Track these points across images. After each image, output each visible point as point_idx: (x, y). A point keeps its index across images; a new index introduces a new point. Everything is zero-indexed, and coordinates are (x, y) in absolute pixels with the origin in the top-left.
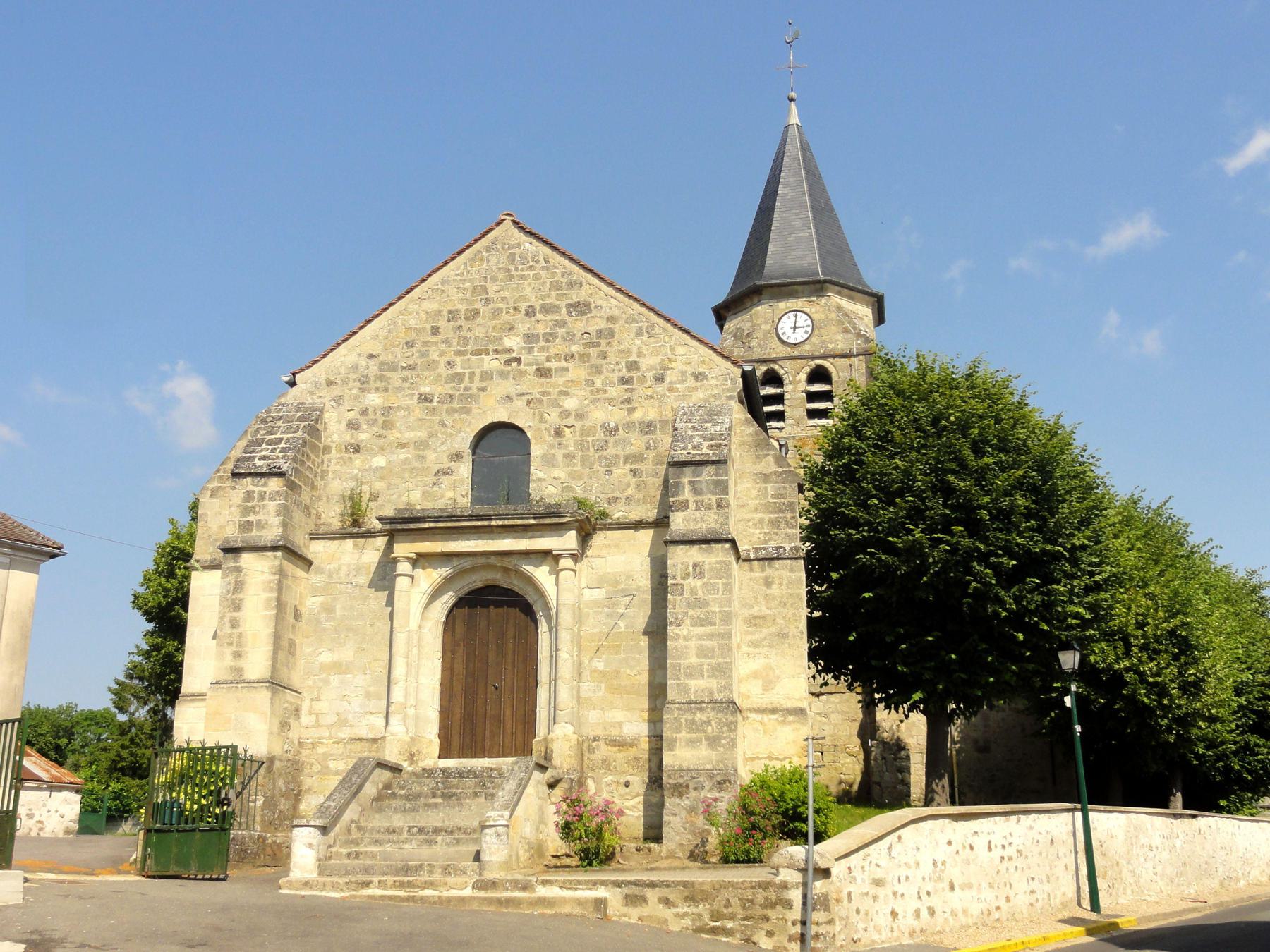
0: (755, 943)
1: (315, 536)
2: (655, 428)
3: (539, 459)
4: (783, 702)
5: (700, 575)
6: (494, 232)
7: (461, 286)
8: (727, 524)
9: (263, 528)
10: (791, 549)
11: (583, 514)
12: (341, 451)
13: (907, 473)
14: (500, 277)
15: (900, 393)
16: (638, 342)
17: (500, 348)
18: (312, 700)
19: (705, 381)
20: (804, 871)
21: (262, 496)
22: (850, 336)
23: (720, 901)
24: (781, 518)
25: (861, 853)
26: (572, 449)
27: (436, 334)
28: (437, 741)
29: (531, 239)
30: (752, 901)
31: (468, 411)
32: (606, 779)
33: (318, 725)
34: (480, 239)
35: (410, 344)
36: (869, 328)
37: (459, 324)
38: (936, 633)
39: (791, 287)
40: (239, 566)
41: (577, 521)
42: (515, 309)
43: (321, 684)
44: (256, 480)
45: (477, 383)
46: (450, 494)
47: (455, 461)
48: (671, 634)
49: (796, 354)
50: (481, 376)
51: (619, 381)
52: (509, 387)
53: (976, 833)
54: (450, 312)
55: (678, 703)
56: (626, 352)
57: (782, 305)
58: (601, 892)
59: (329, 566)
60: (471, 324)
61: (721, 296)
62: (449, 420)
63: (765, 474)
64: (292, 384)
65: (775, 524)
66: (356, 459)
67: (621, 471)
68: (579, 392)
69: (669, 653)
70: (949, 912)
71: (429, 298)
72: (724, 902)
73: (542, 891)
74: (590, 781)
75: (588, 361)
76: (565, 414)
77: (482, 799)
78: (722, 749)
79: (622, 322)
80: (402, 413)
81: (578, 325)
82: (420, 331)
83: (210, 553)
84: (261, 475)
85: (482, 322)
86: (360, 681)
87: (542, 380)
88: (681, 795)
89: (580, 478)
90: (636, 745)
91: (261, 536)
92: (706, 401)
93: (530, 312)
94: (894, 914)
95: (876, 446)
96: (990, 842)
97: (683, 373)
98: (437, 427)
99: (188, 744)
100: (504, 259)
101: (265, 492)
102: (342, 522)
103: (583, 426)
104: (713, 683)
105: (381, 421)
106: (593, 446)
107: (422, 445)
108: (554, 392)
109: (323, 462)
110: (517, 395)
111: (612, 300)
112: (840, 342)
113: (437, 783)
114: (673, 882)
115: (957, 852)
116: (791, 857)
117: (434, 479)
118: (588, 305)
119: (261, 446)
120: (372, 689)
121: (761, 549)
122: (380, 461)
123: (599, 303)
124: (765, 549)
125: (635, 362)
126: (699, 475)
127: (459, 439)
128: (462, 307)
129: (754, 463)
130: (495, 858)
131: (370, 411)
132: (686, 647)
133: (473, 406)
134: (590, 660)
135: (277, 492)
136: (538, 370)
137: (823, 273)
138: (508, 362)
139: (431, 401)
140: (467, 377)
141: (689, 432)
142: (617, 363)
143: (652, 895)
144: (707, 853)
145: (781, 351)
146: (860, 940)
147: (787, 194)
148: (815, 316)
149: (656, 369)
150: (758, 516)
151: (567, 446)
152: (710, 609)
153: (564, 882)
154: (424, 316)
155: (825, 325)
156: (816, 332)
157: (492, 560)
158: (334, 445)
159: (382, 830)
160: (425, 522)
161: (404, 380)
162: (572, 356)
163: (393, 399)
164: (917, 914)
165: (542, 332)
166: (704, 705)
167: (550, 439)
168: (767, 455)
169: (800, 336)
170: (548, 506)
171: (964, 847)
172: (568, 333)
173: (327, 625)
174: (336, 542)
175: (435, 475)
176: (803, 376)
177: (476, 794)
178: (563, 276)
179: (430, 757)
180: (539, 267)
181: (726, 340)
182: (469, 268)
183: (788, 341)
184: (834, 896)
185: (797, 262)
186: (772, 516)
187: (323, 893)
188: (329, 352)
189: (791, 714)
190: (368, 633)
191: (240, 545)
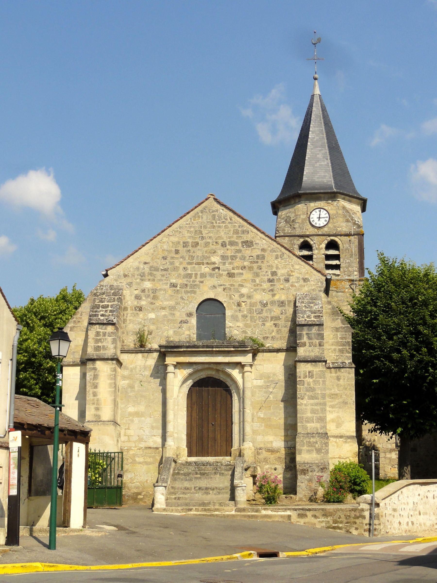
0: (350, 533)
1: (123, 352)
2: (285, 304)
3: (230, 317)
4: (345, 433)
5: (311, 376)
6: (205, 203)
7: (189, 230)
8: (323, 354)
9: (106, 349)
10: (349, 363)
11: (256, 347)
12: (132, 310)
13: (398, 325)
14: (208, 226)
15: (394, 283)
16: (276, 262)
17: (209, 262)
18: (126, 429)
19: (308, 283)
20: (371, 504)
21: (104, 334)
22: (349, 224)
23: (337, 516)
24: (344, 348)
25: (389, 498)
26: (246, 313)
27: (177, 254)
28: (186, 449)
29: (223, 208)
30: (349, 516)
31: (195, 292)
32: (266, 467)
33: (129, 441)
34: (198, 206)
35: (164, 258)
36: (360, 219)
37: (188, 249)
38: (409, 400)
39: (317, 195)
40: (95, 367)
41: (253, 349)
42: (216, 243)
43: (130, 422)
44: (101, 326)
45: (199, 279)
46: (187, 333)
47: (189, 317)
48: (299, 403)
49: (320, 233)
50: (201, 276)
51: (267, 281)
52: (214, 281)
53: (429, 491)
54: (184, 243)
55: (303, 434)
56: (270, 266)
57: (312, 205)
58: (288, 513)
59: (130, 366)
60: (195, 249)
61: (275, 195)
62: (185, 296)
63: (336, 328)
64: (106, 275)
65: (341, 351)
66: (140, 314)
67: (269, 324)
68: (248, 285)
69: (298, 412)
70: (419, 523)
71: (173, 235)
72: (338, 517)
73: (264, 512)
74: (258, 468)
75: (253, 270)
76: (242, 295)
77: (218, 476)
78: (322, 454)
79: (268, 252)
80: (162, 292)
81: (247, 252)
82: (170, 252)
83: (71, 358)
84: (104, 324)
85: (200, 248)
86: (149, 420)
87: (230, 279)
88: (305, 474)
89: (250, 327)
90: (279, 452)
91: (105, 354)
92: (309, 292)
93: (224, 245)
94: (400, 523)
95: (383, 311)
96: (434, 495)
97: (298, 278)
98: (180, 300)
99: (95, 451)
100: (210, 217)
101: (106, 332)
102: (134, 344)
103: (251, 302)
104: (318, 425)
105: (152, 295)
106: (256, 312)
107: (172, 308)
108: (236, 285)
109: (124, 315)
110: (219, 285)
111: (264, 240)
112: (344, 227)
113: (195, 468)
114: (318, 509)
115: (422, 499)
116: (365, 499)
117: (179, 325)
118: (252, 242)
119: (99, 308)
120: (154, 424)
121: (335, 363)
122: (152, 316)
123: (257, 242)
124: (337, 363)
125: (275, 272)
126: (311, 331)
127: (190, 306)
128: (190, 241)
129: (332, 323)
130: (242, 499)
131: (146, 290)
132: (306, 409)
133: (197, 290)
134: (257, 413)
135: (112, 332)
136: (228, 273)
137: (336, 187)
138: (214, 269)
139: (176, 287)
140: (194, 275)
141: (304, 309)
142: (267, 272)
143: (309, 514)
144: (316, 498)
145: (311, 231)
146: (389, 532)
147: (314, 138)
148: (331, 212)
149: (285, 276)
150: (334, 347)
151: (243, 312)
152: (316, 392)
153: (273, 509)
154: (171, 244)
155: (336, 217)
156: (331, 221)
157: (212, 366)
158: (129, 307)
159: (183, 488)
160: (182, 348)
161: (163, 276)
162: (245, 267)
163: (157, 285)
164: (408, 523)
165: (230, 255)
166: (314, 435)
167: (235, 307)
168: (337, 319)
169: (322, 223)
170: (238, 342)
171: (424, 497)
172: (242, 256)
173: (131, 394)
174: (134, 355)
175: (180, 323)
176: (323, 246)
177: (215, 473)
178: (239, 227)
179: (184, 457)
180: (227, 222)
181: (280, 223)
182: (193, 221)
183: (316, 225)
184: (380, 514)
185: (320, 180)
186: (340, 347)
187: (172, 513)
188: (124, 260)
189: (349, 439)
190: (151, 398)
191: (95, 357)
